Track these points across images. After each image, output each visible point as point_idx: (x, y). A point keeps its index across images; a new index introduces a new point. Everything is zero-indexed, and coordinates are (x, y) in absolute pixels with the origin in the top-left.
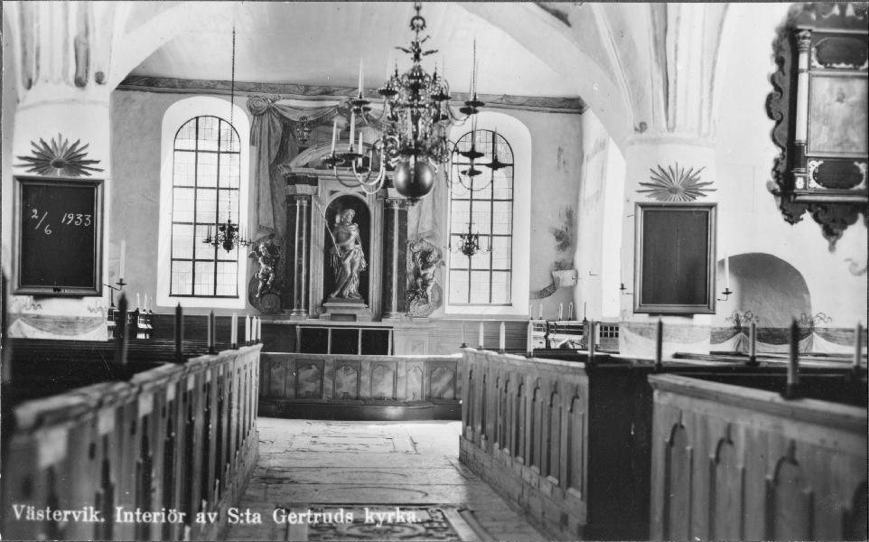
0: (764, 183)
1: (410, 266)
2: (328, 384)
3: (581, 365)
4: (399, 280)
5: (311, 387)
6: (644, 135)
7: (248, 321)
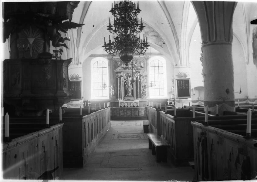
0: (201, 73)
1: (142, 88)
2: (126, 113)
3: (156, 109)
4: (140, 92)
5: (122, 114)
6: (177, 67)
7: (107, 103)
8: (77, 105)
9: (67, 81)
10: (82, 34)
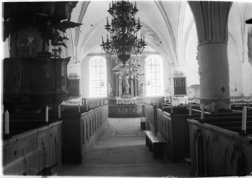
0: (197, 72)
1: (139, 87)
2: (123, 111)
3: (153, 107)
4: (137, 90)
5: (120, 112)
6: (173, 65)
7: (105, 101)
8: (75, 103)
9: (66, 80)
10: (80, 33)
